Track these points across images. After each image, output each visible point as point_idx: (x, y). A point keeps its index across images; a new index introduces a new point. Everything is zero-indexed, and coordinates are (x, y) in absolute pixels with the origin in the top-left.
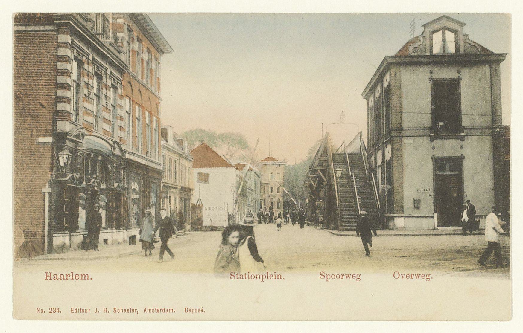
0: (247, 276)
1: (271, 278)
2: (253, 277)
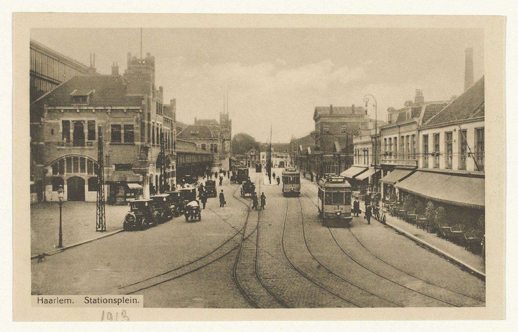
0: (100, 301)
1: (61, 302)
2: (105, 301)
